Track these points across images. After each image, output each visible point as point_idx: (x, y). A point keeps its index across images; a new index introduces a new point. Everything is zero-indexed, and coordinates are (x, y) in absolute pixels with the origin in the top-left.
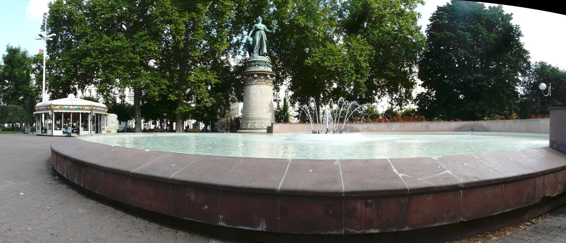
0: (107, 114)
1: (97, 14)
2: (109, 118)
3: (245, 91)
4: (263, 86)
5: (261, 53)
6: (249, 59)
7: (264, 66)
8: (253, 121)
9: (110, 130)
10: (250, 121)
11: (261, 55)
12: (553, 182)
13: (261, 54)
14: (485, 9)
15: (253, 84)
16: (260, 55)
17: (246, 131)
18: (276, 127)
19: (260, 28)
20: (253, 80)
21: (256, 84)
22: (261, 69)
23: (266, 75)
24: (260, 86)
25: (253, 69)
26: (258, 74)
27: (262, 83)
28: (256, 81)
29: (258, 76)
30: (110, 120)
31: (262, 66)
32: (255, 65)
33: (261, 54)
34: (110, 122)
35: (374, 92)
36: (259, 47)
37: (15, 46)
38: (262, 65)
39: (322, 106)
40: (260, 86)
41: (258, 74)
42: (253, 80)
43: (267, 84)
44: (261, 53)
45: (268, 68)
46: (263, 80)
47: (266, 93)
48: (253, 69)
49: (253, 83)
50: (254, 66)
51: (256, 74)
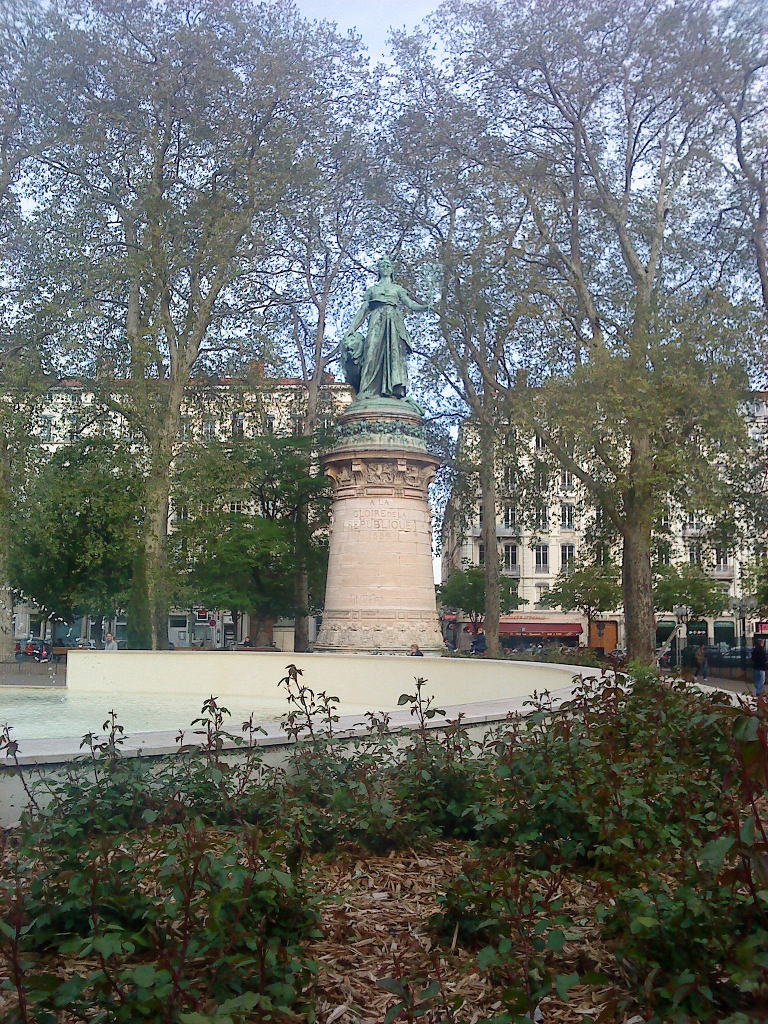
1: (738, 883)
3: (332, 519)
4: (383, 500)
5: (384, 386)
8: (350, 624)
10: (339, 623)
11: (384, 396)
13: (384, 391)
15: (351, 497)
19: (382, 299)
20: (352, 481)
21: (360, 495)
22: (378, 443)
23: (394, 462)
24: (372, 502)
25: (353, 443)
26: (365, 461)
27: (379, 491)
28: (361, 483)
31: (380, 431)
33: (384, 391)
35: (695, 157)
36: (378, 366)
38: (381, 428)
40: (372, 502)
41: (410, 462)
42: (352, 481)
43: (399, 495)
44: (384, 386)
45: (403, 440)
46: (385, 481)
47: (395, 525)
48: (353, 443)
49: (352, 492)
50: (355, 433)
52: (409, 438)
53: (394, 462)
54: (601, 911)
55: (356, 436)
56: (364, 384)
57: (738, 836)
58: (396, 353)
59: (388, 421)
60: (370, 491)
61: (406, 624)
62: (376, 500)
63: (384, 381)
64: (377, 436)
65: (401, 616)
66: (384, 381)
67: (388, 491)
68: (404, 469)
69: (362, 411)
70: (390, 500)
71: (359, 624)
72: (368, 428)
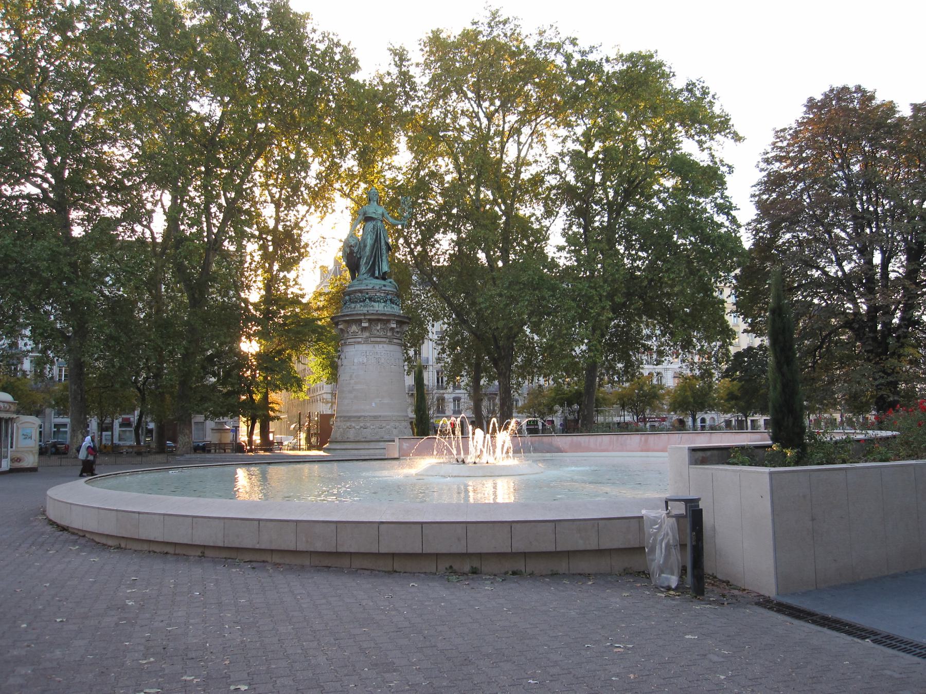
0: (15, 416)
2: (17, 426)
4: (381, 346)
6: (349, 287)
7: (384, 302)
8: (362, 425)
9: (19, 455)
11: (377, 278)
12: (856, 289)
13: (377, 275)
14: (897, 116)
15: (359, 343)
16: (373, 275)
17: (338, 447)
18: (405, 444)
19: (374, 216)
23: (360, 321)
26: (370, 321)
27: (379, 339)
29: (370, 324)
30: (21, 432)
31: (378, 301)
32: (364, 301)
34: (21, 437)
37: (360, 72)
39: (608, 73)
41: (370, 321)
50: (361, 302)
51: (365, 319)
52: (395, 306)
53: (360, 321)
54: (12, 109)
55: (362, 304)
56: (363, 269)
57: (673, 590)
58: (384, 251)
59: (382, 295)
60: (372, 339)
61: (397, 424)
62: (376, 346)
63: (377, 268)
64: (376, 305)
65: (394, 418)
66: (377, 268)
67: (384, 340)
68: (394, 326)
69: (365, 288)
70: (385, 346)
71: (368, 425)
72: (370, 299)
